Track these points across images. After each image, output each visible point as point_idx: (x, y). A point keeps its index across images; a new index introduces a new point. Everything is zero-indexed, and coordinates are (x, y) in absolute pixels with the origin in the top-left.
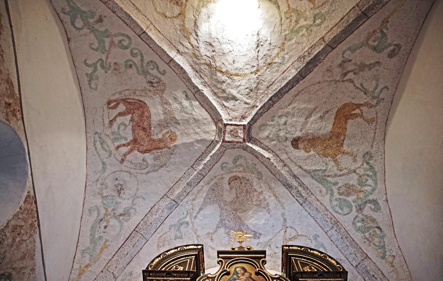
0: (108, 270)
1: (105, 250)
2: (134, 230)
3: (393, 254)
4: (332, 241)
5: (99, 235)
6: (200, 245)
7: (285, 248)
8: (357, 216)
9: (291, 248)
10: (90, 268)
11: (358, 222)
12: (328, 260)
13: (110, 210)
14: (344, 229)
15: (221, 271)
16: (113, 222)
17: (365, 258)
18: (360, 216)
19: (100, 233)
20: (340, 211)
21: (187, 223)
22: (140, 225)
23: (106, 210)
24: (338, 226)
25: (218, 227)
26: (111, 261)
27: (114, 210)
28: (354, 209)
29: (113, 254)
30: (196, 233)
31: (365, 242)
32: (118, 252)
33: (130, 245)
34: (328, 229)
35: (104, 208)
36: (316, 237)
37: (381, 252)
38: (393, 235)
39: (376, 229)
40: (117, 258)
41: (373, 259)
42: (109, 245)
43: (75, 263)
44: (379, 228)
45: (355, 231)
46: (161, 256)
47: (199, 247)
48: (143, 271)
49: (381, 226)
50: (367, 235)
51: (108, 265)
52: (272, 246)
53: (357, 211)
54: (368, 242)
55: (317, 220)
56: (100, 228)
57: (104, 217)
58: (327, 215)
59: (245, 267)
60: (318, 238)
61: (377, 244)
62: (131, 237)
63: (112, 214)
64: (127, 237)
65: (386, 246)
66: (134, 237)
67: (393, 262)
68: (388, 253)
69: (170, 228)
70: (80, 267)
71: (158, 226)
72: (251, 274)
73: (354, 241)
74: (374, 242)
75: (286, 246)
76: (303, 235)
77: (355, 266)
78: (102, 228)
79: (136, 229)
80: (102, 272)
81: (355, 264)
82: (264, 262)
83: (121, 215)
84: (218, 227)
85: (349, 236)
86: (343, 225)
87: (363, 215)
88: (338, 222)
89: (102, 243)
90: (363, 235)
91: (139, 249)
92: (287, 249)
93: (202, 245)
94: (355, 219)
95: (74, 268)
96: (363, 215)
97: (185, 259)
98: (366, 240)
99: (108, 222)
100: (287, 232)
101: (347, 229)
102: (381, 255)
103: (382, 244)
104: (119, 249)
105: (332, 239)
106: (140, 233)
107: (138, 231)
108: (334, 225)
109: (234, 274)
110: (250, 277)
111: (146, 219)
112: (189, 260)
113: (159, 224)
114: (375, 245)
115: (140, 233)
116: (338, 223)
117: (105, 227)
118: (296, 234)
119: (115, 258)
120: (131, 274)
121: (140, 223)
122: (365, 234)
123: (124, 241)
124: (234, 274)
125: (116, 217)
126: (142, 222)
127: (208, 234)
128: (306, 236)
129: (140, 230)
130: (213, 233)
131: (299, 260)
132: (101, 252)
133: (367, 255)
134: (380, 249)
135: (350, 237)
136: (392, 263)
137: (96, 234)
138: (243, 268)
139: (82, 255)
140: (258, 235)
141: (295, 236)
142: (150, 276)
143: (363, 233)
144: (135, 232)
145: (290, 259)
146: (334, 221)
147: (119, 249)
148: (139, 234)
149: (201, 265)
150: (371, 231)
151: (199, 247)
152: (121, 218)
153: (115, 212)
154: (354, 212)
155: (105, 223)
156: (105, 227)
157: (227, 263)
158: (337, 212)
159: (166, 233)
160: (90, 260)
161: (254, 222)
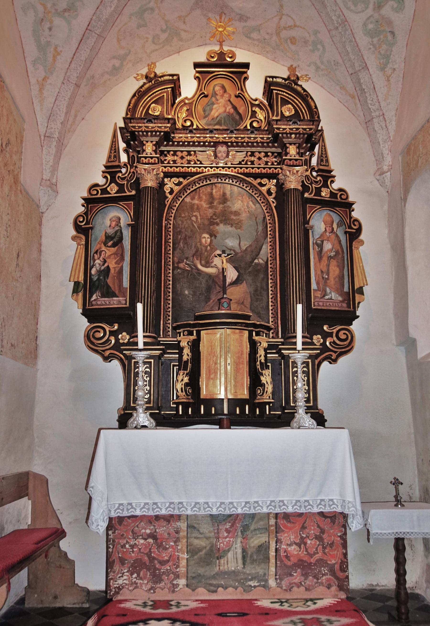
0: (68, 81)
1: (58, 57)
2: (87, 29)
3: (395, 67)
4: (333, 41)
5: (45, 40)
6: (176, 75)
7: (268, 79)
8: (372, 16)
9: (274, 79)
10: (49, 81)
11: (371, 23)
12: (308, 101)
13: (49, 5)
14: (351, 30)
15: (198, 93)
16: (58, 21)
17: (363, 68)
18: (376, 16)
19: (46, 38)
20: (353, 7)
21: (152, 9)
22: (93, 21)
23: (44, 6)
24: (345, 26)
25: (192, 9)
26: (69, 71)
27: (54, 5)
28: (371, 6)
29: (69, 61)
30: (163, 19)
31: (370, 49)
32: (75, 59)
33: (87, 50)
34: (332, 28)
35: (41, 4)
36: (316, 32)
37: (383, 62)
38: (406, 42)
39: (389, 34)
40: (76, 66)
41: (370, 71)
42: (61, 51)
43: (30, 78)
44: (392, 33)
45: (363, 35)
46: (137, 95)
47: (175, 78)
48: (124, 119)
49: (396, 33)
50: (375, 40)
51: (67, 74)
52: (261, 31)
53: (374, 9)
54: (373, 49)
55: (321, 14)
56: (44, 31)
57: (44, 16)
58: (335, 11)
59: (225, 85)
60: (318, 34)
61: (383, 52)
62: (84, 38)
63: (54, 11)
64: (80, 39)
65: (392, 56)
66: (88, 38)
67: (390, 76)
68: (390, 65)
69: (130, 18)
70: (37, 81)
71: (115, 19)
72: (230, 96)
73: (358, 46)
74: (381, 49)
75: (270, 77)
76: (301, 27)
77: (350, 73)
78: (47, 30)
79: (89, 28)
80: (64, 83)
81: (351, 71)
82: (246, 78)
83: (65, 10)
84: (192, 9)
85: (354, 40)
86: (351, 25)
87: (380, 15)
88: (346, 21)
89: (52, 49)
90: (371, 40)
91: (97, 50)
92: (270, 81)
93: (178, 75)
94: (368, 19)
95: (31, 84)
96: (380, 15)
97: (160, 93)
98: (372, 47)
99: (51, 22)
100: (282, 20)
101: (354, 31)
102: (382, 66)
103: (388, 53)
104: (74, 55)
105: (333, 39)
106: (95, 33)
107: (92, 29)
108: (340, 25)
109: (212, 96)
110: (229, 100)
111: (98, 12)
112: (165, 94)
113: (116, 17)
114: (381, 54)
115: (95, 33)
116: (346, 23)
117: (50, 29)
118: (293, 24)
119: (73, 65)
120: (93, 77)
121: (91, 19)
122: (373, 40)
123: (77, 44)
124: (212, 96)
125: (61, 14)
126: (94, 18)
127: (180, 17)
128: (304, 28)
129: (93, 28)
130: (187, 16)
131: (281, 94)
132: (54, 60)
133: (366, 64)
134: (383, 59)
135: (356, 41)
136: (388, 77)
137: (42, 39)
138: (223, 87)
139: (33, 66)
140: (245, 18)
141: (291, 26)
142: (131, 123)
143: (372, 38)
144: (88, 31)
145: (272, 92)
146: (341, 20)
147: (74, 55)
148: (94, 34)
149: (254, 538)
150: (382, 36)
151: (175, 78)
152: (66, 14)
153: (56, 7)
154: (370, 11)
155: (48, 23)
156: (50, 29)
157: (205, 82)
158: (348, 8)
159: (126, 24)
160: (45, 71)
161: (241, 5)
